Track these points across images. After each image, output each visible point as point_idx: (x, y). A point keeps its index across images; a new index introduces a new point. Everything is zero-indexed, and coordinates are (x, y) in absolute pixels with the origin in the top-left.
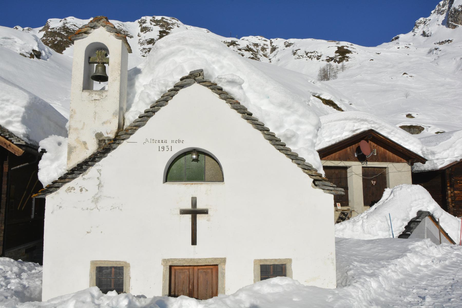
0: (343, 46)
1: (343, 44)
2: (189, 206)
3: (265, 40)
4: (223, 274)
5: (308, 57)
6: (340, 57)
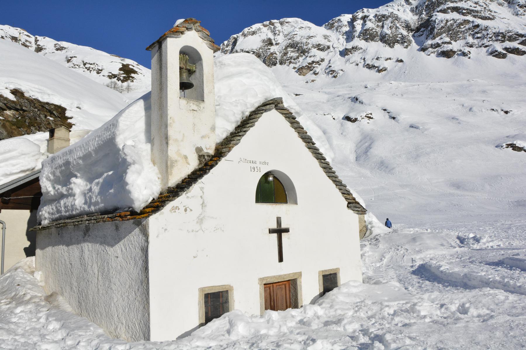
0: (129, 65)
1: (128, 61)
2: (274, 226)
3: (28, 36)
4: (301, 286)
5: (86, 68)
6: (125, 75)
